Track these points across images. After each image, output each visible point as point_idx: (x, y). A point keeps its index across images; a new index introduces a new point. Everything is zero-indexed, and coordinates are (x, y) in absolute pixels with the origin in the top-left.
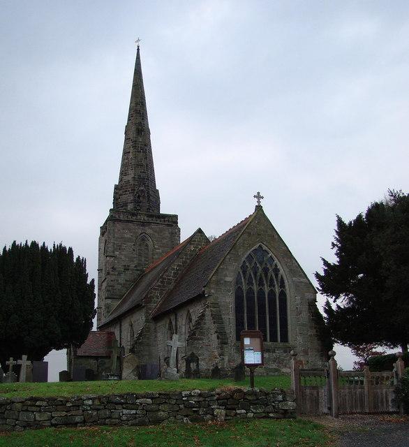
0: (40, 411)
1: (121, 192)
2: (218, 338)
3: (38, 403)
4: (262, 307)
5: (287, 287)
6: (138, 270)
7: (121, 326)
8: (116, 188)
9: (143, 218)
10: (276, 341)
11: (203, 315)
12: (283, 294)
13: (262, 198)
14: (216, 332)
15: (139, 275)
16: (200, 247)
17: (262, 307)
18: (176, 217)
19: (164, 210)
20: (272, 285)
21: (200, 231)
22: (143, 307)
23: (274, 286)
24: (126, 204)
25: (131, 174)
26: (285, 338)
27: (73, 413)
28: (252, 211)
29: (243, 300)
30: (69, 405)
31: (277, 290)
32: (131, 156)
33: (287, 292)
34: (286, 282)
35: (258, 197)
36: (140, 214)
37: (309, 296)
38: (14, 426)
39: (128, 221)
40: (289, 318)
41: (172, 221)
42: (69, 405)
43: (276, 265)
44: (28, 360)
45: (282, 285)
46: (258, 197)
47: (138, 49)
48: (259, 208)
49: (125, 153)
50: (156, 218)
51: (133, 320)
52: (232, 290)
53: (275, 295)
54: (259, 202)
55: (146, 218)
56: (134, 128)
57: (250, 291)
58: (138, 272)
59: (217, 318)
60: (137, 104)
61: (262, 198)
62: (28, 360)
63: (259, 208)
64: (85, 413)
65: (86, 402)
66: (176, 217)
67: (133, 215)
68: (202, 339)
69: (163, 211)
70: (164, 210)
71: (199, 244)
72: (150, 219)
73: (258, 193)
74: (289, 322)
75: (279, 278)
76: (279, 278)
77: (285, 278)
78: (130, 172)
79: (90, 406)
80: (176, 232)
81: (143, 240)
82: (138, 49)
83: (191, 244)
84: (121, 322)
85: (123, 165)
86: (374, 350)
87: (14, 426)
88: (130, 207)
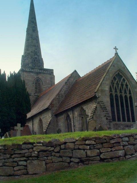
0: (90, 149)
1: (25, 58)
2: (107, 119)
3: (87, 142)
4: (126, 101)
5: (132, 94)
6: (36, 96)
7: (33, 121)
10: (130, 121)
11: (96, 108)
12: (131, 97)
13: (118, 49)
14: (105, 116)
15: (36, 98)
16: (76, 79)
17: (126, 101)
18: (53, 70)
19: (46, 66)
20: (125, 92)
21: (75, 71)
22: (50, 109)
27: (117, 148)
28: (113, 55)
30: (112, 142)
31: (128, 96)
33: (133, 96)
35: (116, 48)
36: (36, 69)
38: (69, 163)
39: (30, 72)
41: (50, 72)
42: (112, 142)
44: (21, 126)
46: (116, 48)
48: (116, 54)
51: (41, 117)
52: (108, 94)
53: (127, 98)
54: (116, 51)
55: (38, 70)
57: (116, 96)
58: (36, 97)
60: (32, 18)
62: (21, 126)
63: (116, 54)
64: (126, 148)
65: (124, 139)
66: (53, 70)
67: (32, 69)
70: (46, 66)
71: (75, 78)
73: (116, 47)
77: (131, 89)
79: (127, 141)
80: (53, 78)
83: (72, 78)
84: (33, 120)
87: (69, 163)
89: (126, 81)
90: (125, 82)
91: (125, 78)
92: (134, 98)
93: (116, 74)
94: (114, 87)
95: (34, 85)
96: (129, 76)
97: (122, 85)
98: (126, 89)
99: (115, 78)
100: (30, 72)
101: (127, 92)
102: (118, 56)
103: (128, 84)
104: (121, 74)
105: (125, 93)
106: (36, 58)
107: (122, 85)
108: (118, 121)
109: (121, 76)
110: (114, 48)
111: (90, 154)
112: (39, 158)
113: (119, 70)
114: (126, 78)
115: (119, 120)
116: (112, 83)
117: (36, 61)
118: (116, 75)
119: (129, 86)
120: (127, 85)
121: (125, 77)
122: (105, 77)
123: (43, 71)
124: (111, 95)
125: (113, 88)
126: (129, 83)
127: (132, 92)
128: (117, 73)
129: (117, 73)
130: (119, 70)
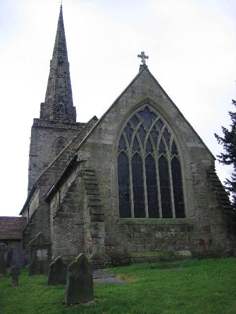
5: (180, 154)
8: (42, 105)
9: (60, 126)
13: (147, 57)
23: (165, 152)
24: (48, 116)
25: (53, 93)
26: (181, 213)
28: (136, 72)
29: (143, 191)
32: (53, 80)
33: (181, 160)
34: (178, 147)
35: (143, 56)
37: (206, 162)
40: (184, 187)
43: (166, 129)
45: (175, 150)
46: (143, 56)
47: (61, 8)
48: (144, 68)
49: (50, 79)
50: (71, 125)
56: (56, 60)
57: (137, 156)
59: (92, 187)
61: (147, 57)
63: (144, 68)
68: (72, 217)
69: (78, 121)
72: (66, 126)
74: (185, 192)
75: (171, 143)
76: (171, 143)
78: (52, 92)
81: (61, 142)
82: (61, 8)
85: (48, 88)
86: (6, 260)
88: (51, 118)
89: (166, 124)
90: (164, 127)
91: (163, 119)
92: (184, 161)
93: (139, 109)
94: (133, 136)
95: (54, 149)
96: (171, 113)
97: (155, 132)
98: (164, 141)
99: (135, 119)
100: (47, 128)
101: (167, 149)
102: (148, 71)
103: (170, 130)
104: (152, 109)
105: (160, 152)
106: (61, 106)
107: (155, 132)
108: (136, 216)
109: (152, 113)
110: (139, 56)
111: (64, 291)
112: (83, 259)
113: (148, 101)
114: (165, 118)
115: (140, 213)
116: (129, 129)
117: (60, 111)
118: (140, 112)
119: (173, 136)
120: (167, 134)
121: (162, 115)
122: (107, 116)
123: (72, 127)
124: (122, 156)
125: (168, 145)
126: (173, 129)
127: (179, 150)
128: (143, 107)
129: (144, 106)
130: (148, 101)
